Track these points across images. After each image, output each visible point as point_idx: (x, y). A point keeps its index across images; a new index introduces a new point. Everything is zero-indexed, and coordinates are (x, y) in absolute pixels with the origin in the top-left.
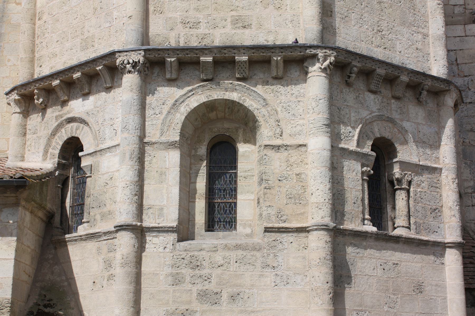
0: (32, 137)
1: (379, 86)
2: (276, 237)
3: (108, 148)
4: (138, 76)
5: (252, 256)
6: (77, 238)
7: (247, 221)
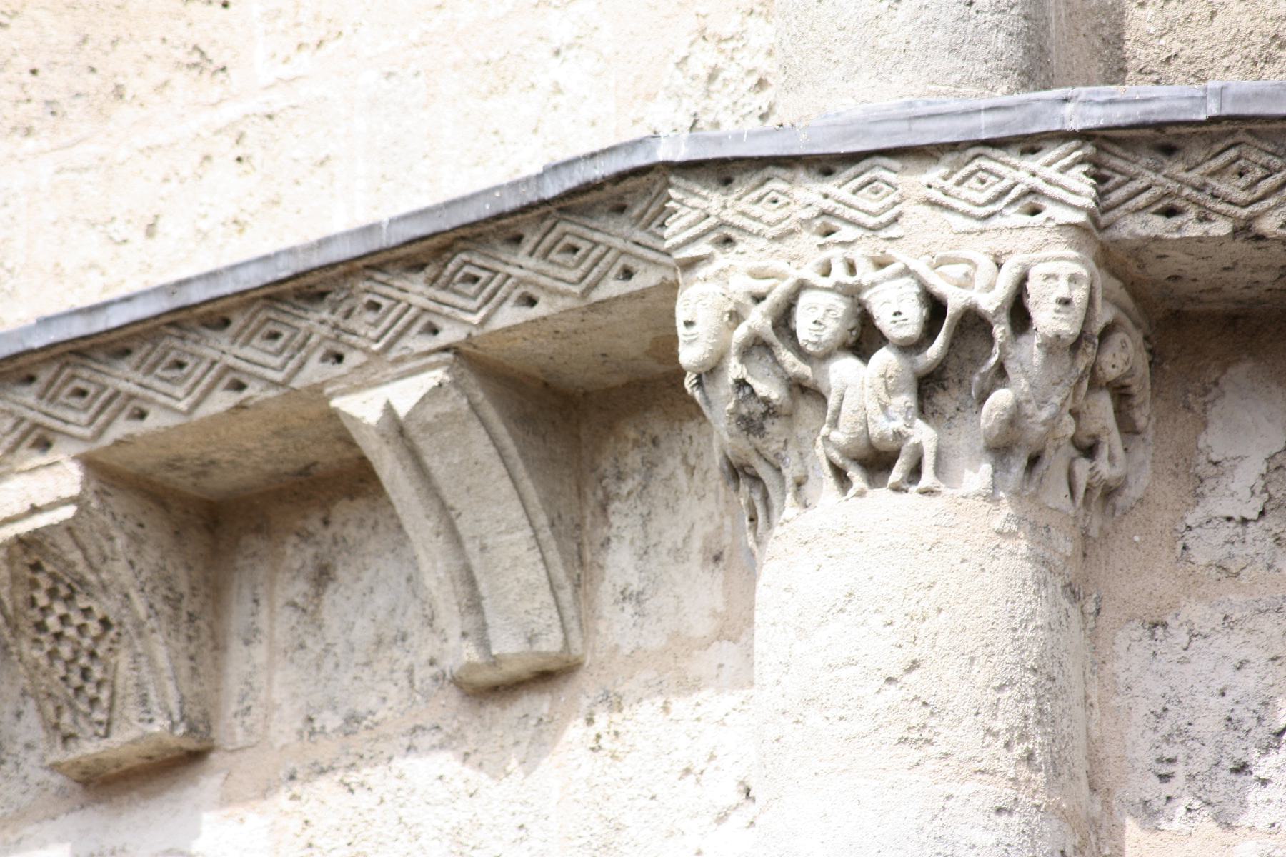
4: (1003, 515)
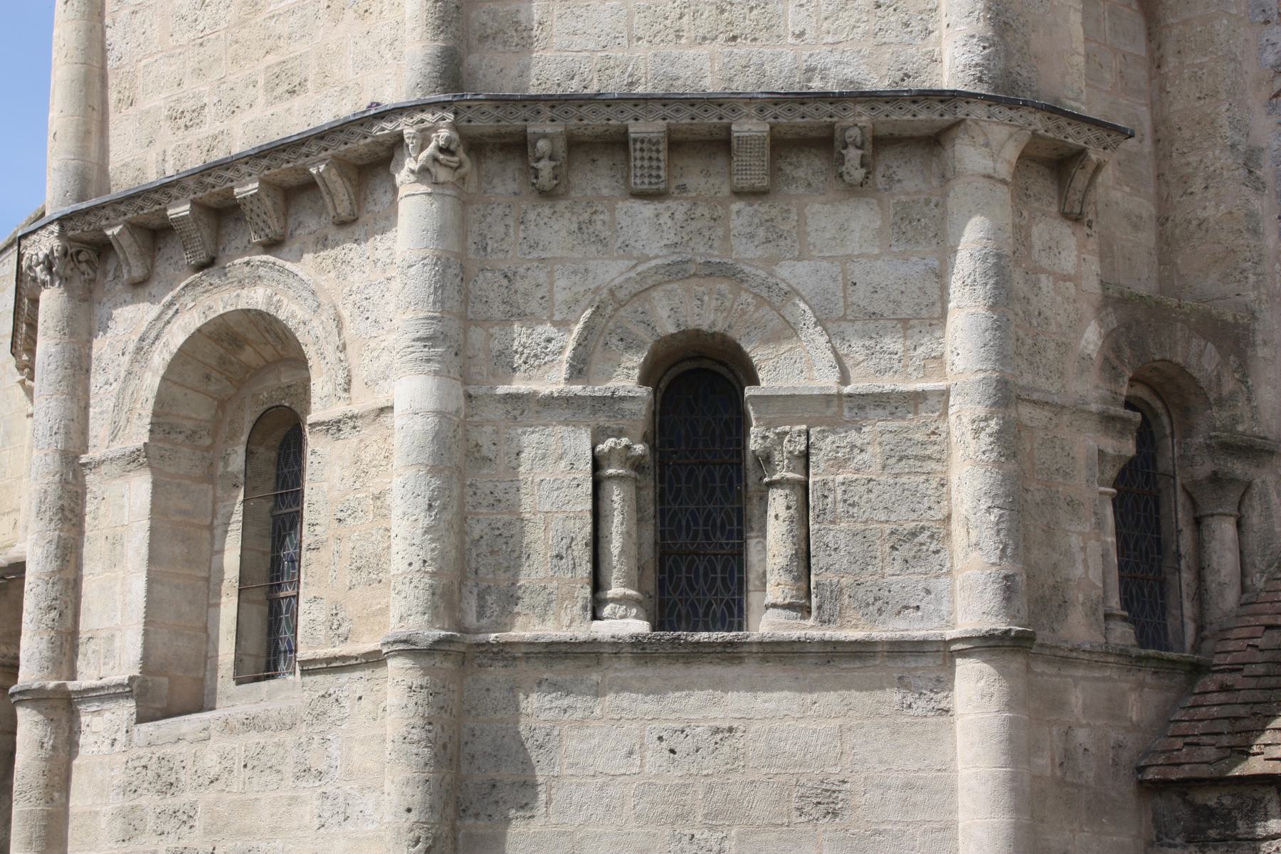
1: (662, 173)
2: (327, 685)
5: (278, 745)
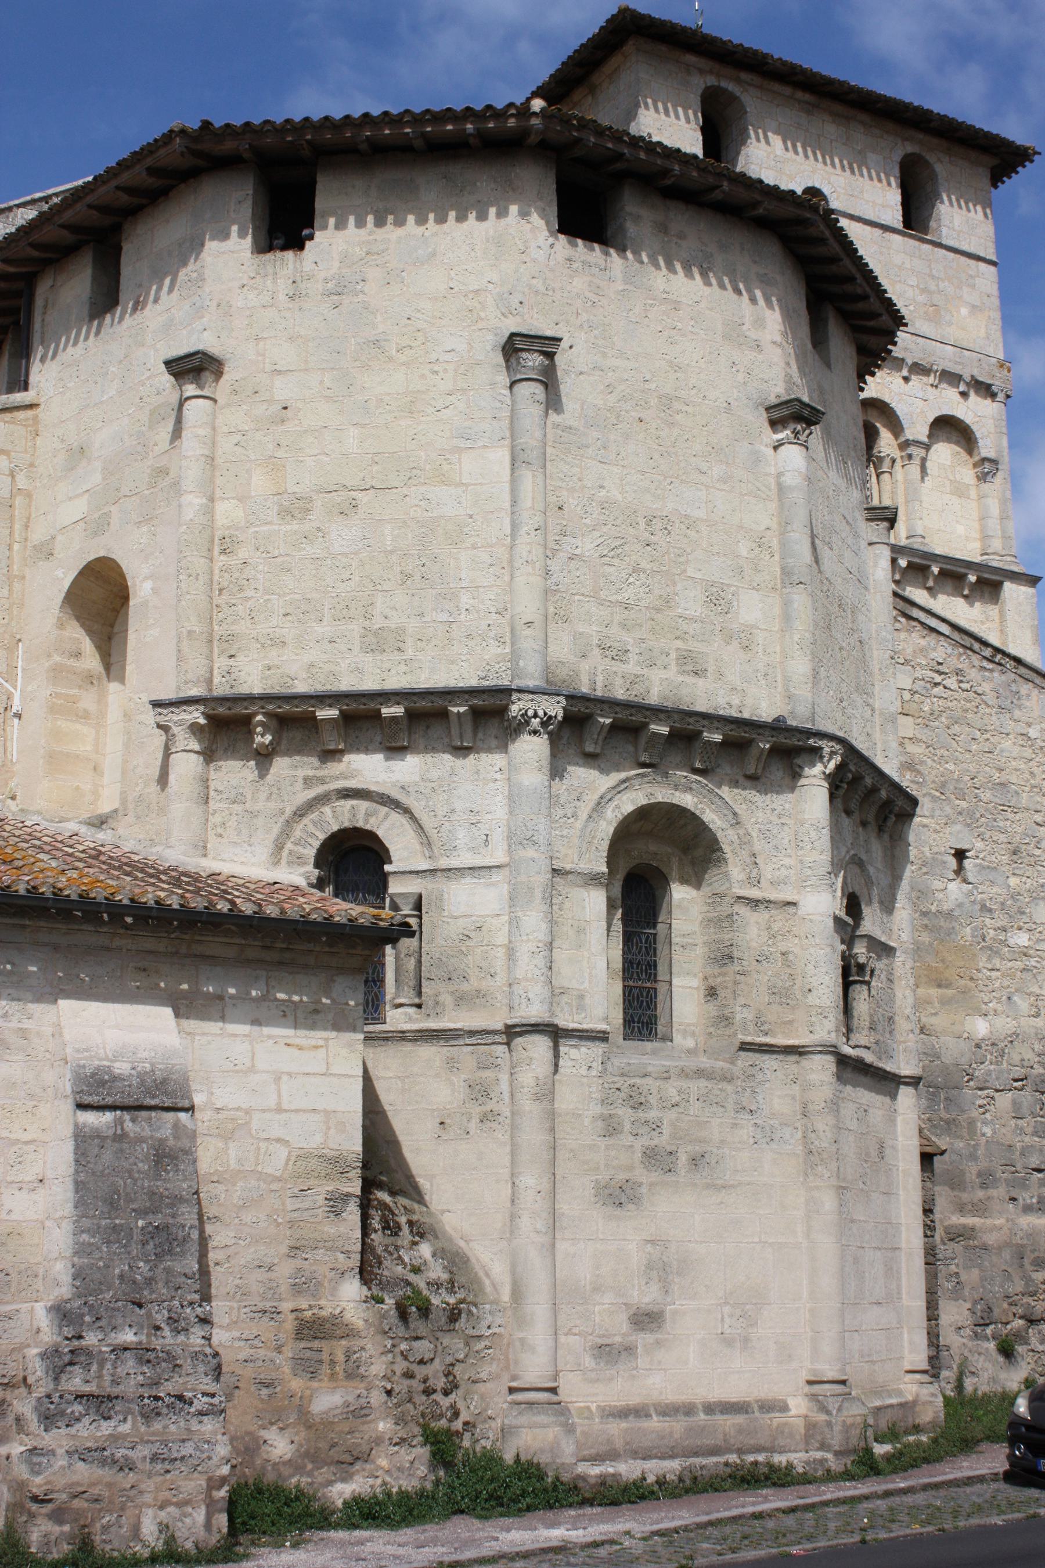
0: (228, 809)
3: (470, 869)
5: (721, 1090)
6: (390, 1035)
7: (689, 1025)
